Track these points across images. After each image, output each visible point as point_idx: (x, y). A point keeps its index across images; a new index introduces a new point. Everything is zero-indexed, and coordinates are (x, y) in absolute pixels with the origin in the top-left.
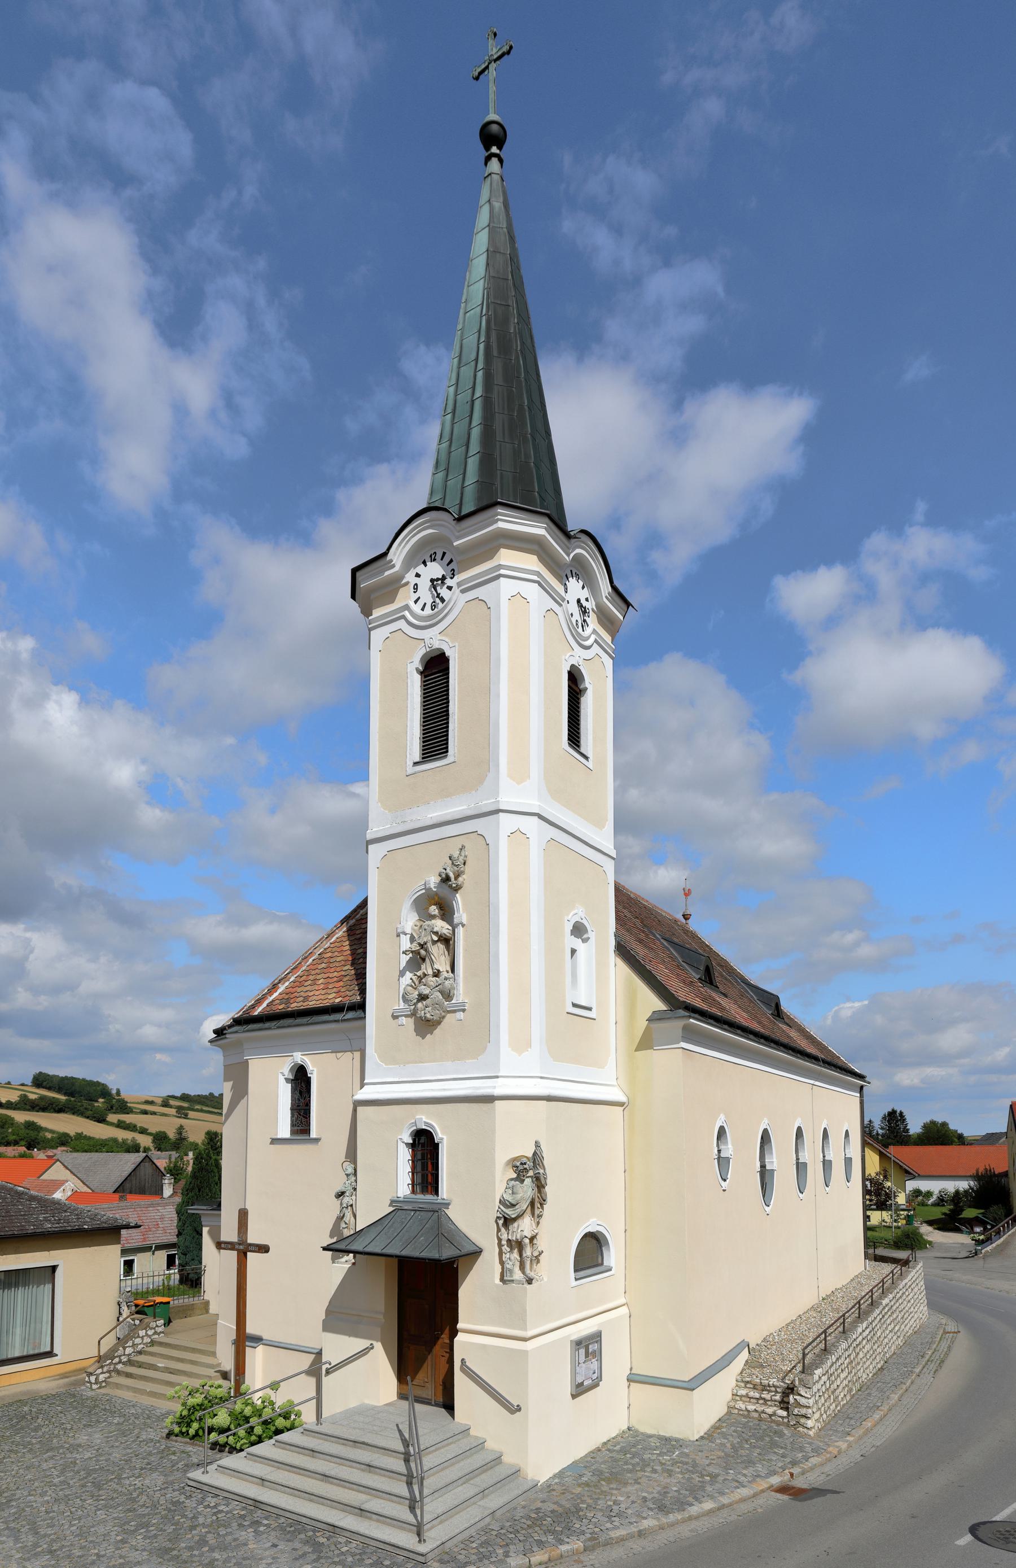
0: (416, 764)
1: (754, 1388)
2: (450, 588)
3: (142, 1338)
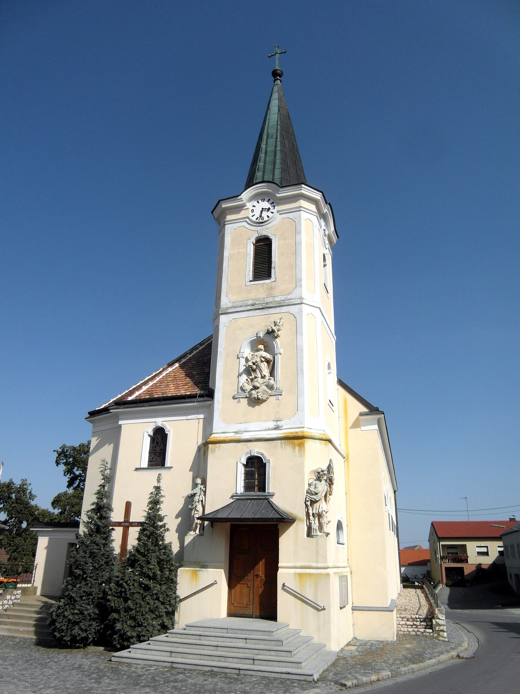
0: (250, 281)
1: (408, 620)
2: (272, 213)
3: (8, 600)
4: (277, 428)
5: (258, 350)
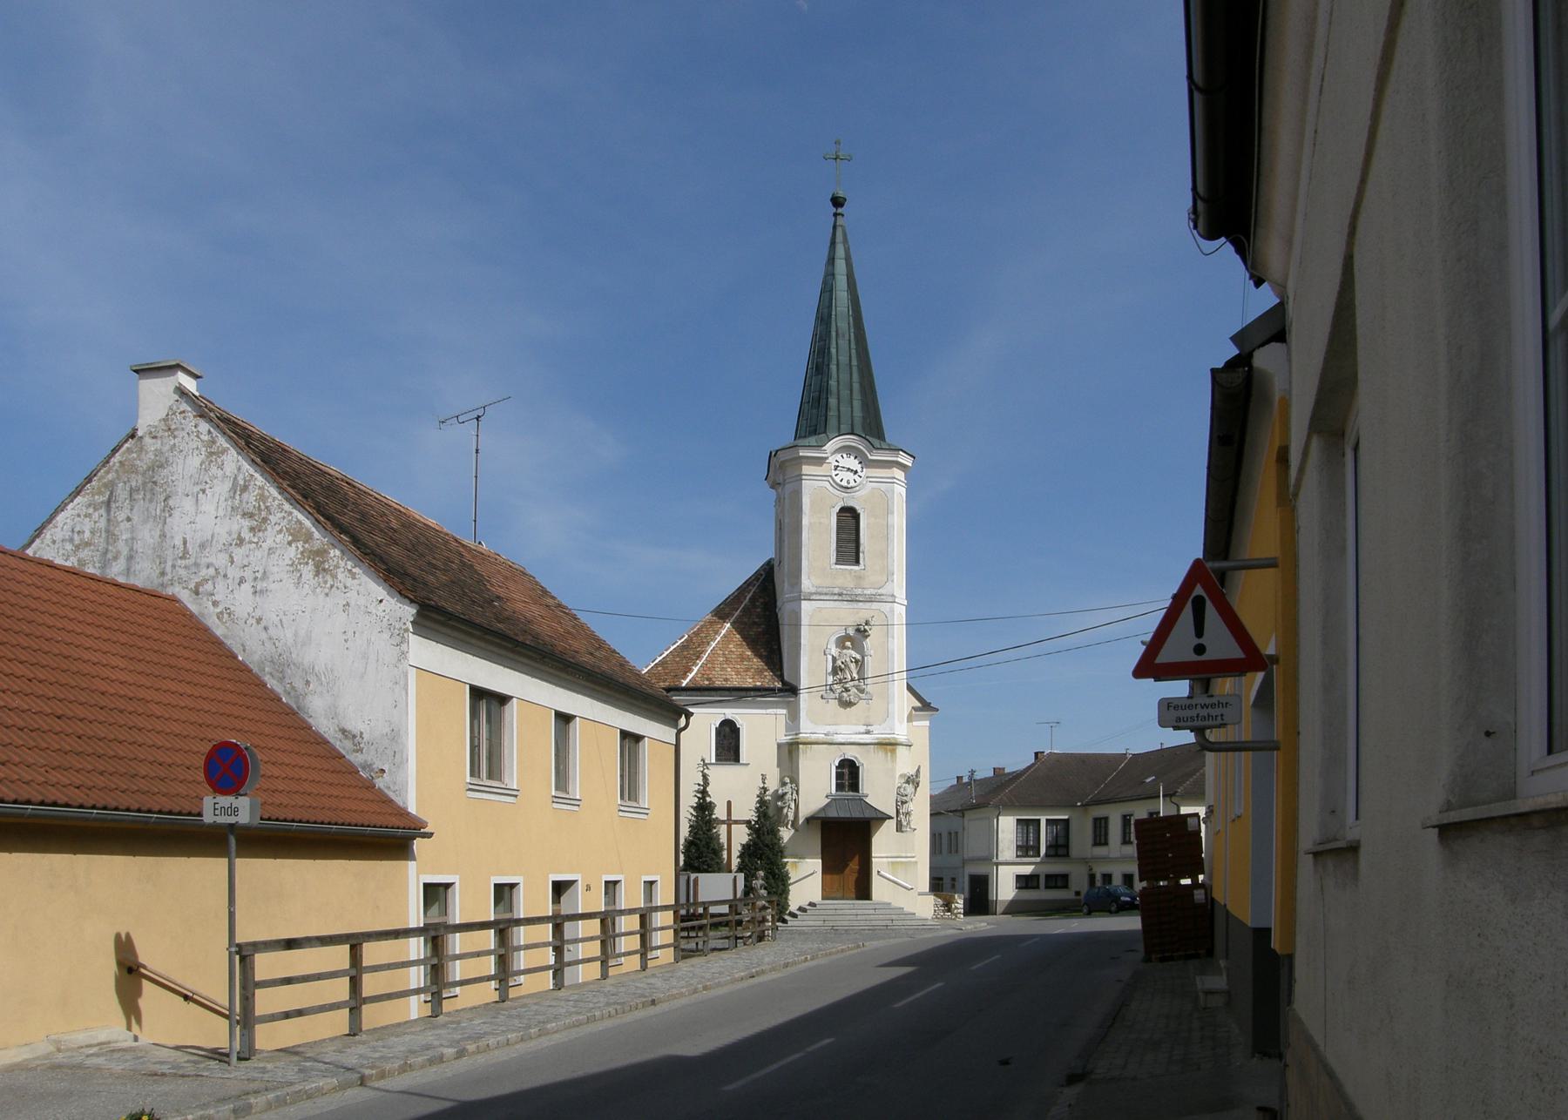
4: (868, 732)
5: (845, 647)
